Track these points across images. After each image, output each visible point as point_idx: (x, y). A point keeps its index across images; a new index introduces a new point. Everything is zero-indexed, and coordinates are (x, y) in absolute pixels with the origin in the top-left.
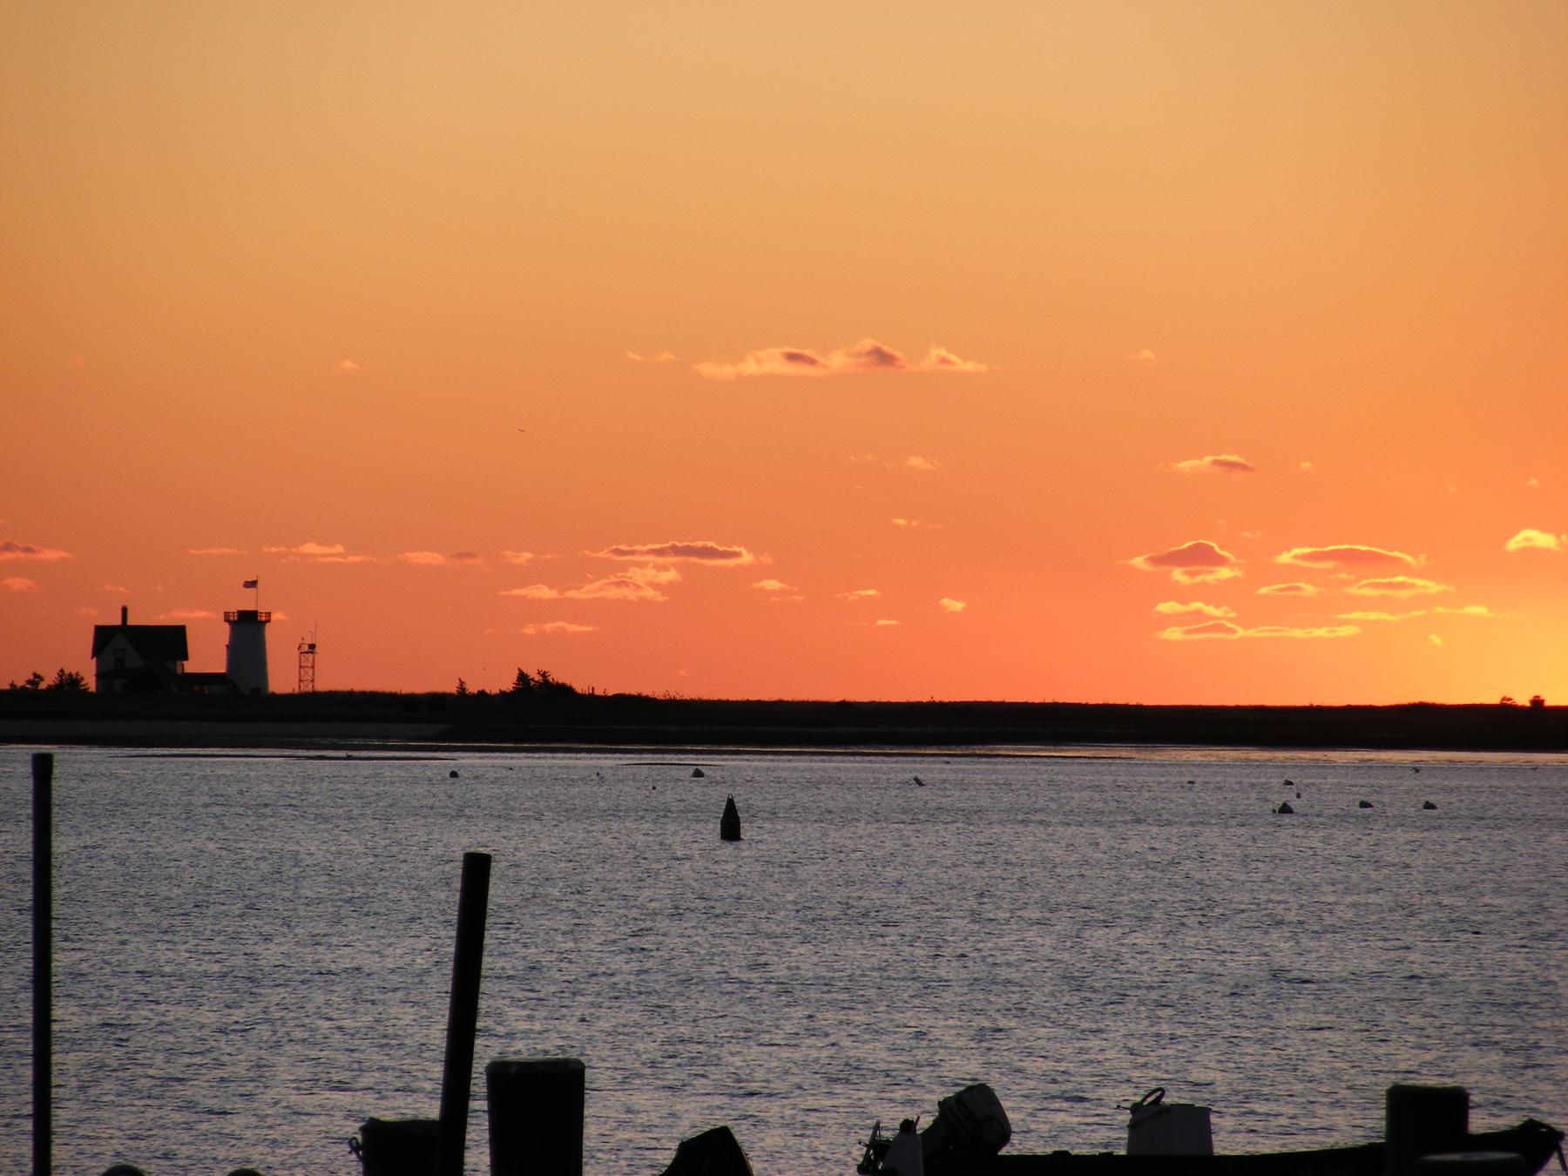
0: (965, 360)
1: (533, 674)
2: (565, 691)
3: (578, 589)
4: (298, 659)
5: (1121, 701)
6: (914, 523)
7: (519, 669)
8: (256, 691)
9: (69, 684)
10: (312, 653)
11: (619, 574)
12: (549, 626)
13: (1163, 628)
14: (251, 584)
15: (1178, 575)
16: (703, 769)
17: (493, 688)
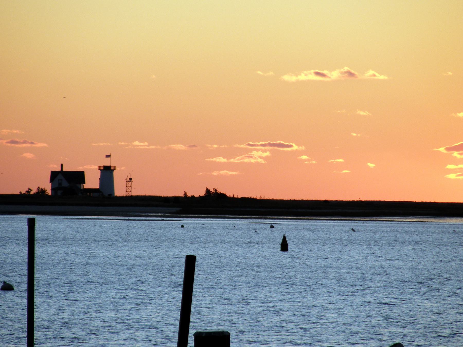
0: (381, 74)
1: (212, 190)
2: (223, 196)
3: (234, 158)
4: (125, 183)
5: (428, 201)
6: (359, 135)
7: (207, 188)
8: (110, 195)
9: (41, 192)
10: (131, 181)
11: (249, 153)
12: (222, 172)
13: (449, 174)
14: (109, 156)
15: (456, 154)
16: (274, 225)
17: (197, 195)
